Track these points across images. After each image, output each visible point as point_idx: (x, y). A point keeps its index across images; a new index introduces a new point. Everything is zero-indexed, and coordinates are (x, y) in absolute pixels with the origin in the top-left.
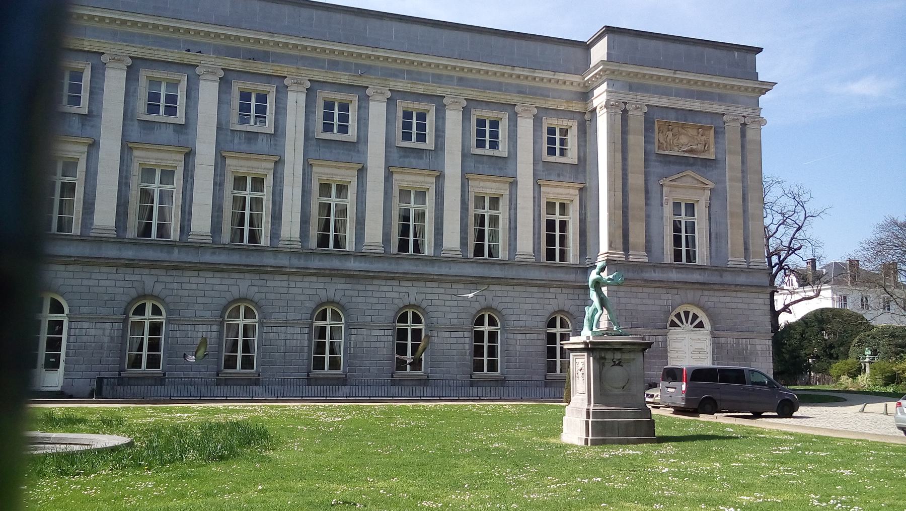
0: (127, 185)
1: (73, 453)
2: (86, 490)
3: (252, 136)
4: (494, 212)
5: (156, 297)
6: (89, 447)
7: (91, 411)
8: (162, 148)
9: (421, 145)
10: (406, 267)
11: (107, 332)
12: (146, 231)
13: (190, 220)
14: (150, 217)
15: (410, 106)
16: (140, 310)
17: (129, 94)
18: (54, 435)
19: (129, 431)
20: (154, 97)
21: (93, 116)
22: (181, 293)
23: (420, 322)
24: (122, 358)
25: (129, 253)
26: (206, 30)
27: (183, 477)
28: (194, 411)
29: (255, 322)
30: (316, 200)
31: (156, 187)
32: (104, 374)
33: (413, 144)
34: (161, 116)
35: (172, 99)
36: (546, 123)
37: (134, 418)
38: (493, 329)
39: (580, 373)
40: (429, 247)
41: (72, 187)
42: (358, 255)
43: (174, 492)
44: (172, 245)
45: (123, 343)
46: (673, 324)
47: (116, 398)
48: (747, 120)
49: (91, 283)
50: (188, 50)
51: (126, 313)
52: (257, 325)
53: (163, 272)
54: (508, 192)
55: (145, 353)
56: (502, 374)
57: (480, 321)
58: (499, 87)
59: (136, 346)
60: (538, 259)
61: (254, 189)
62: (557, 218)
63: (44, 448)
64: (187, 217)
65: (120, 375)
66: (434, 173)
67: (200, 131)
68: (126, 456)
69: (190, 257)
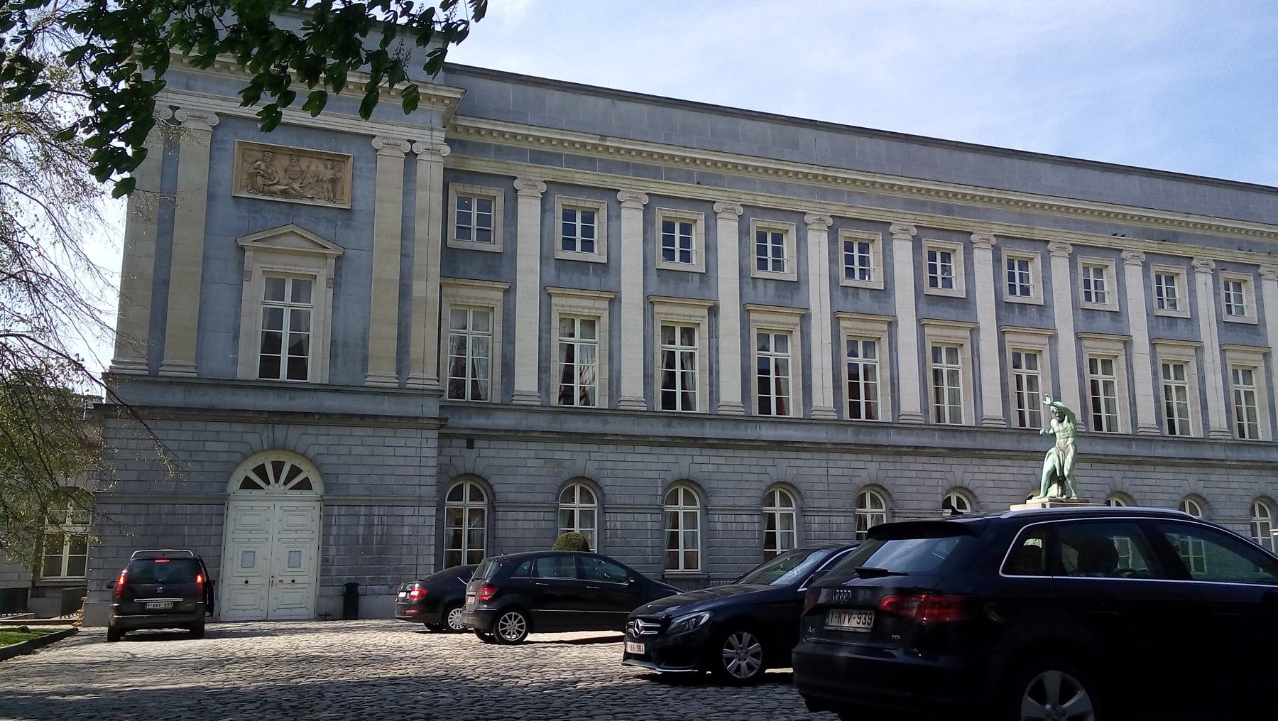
3: (1022, 306)
4: (1108, 378)
10: (768, 433)
15: (673, 214)
33: (578, 254)
36: (928, 244)
42: (806, 422)
46: (248, 484)
52: (486, 509)
56: (704, 571)
58: (590, 163)
61: (1029, 368)
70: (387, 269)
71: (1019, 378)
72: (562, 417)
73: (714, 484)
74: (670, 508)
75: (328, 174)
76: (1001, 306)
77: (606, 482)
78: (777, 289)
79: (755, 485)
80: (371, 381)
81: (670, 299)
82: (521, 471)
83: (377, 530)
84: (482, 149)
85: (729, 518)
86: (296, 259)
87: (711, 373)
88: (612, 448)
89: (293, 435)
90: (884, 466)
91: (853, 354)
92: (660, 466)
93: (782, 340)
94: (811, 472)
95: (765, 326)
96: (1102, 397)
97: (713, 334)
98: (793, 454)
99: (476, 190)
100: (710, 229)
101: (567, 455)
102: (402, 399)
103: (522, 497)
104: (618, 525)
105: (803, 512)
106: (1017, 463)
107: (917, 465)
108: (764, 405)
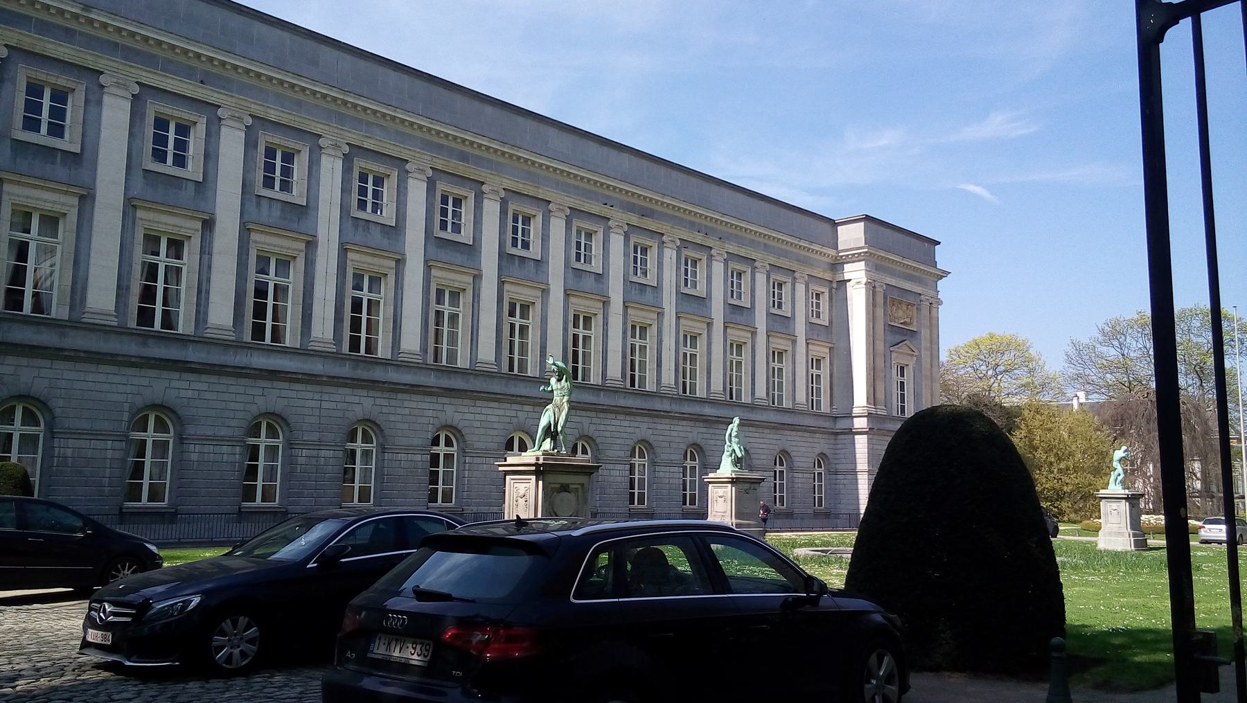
4: (587, 332)
8: (24, 180)
9: (178, 172)
15: (168, 111)
23: (38, 425)
29: (453, 450)
30: (139, 256)
38: (161, 437)
39: (522, 501)
40: (293, 335)
42: (302, 352)
54: (76, 210)
60: (425, 359)
66: (471, 271)
69: (74, 341)
71: (512, 326)
74: (252, 441)
76: (502, 255)
77: (57, 404)
78: (283, 211)
85: (206, 449)
87: (199, 291)
90: (378, 401)
91: (358, 287)
92: (129, 389)
94: (305, 405)
95: (267, 248)
96: (517, 339)
97: (206, 250)
98: (286, 385)
104: (69, 452)
105: (290, 445)
108: (258, 331)
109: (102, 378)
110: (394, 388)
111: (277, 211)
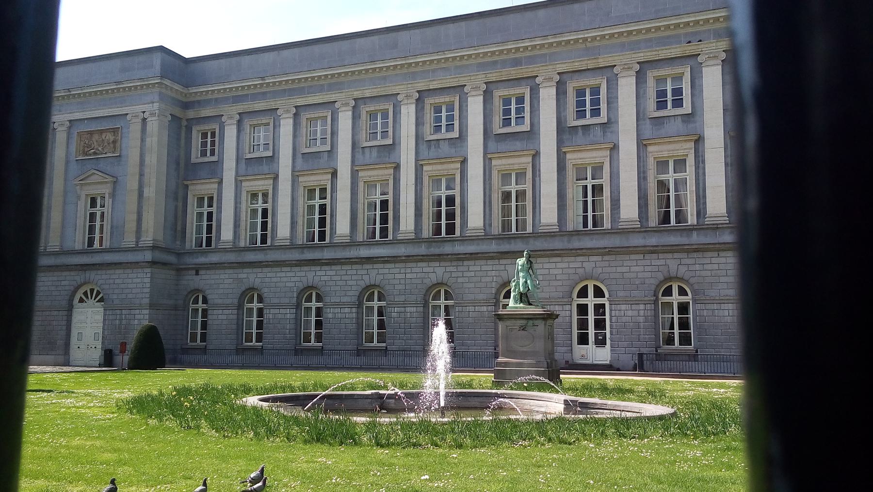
0: (645, 178)
1: (627, 419)
2: (642, 452)
5: (681, 279)
6: (638, 415)
7: (637, 383)
8: (672, 140)
11: (642, 313)
12: (666, 218)
13: (705, 203)
14: (668, 206)
16: (668, 292)
17: (419, 123)
18: (609, 402)
19: (671, 402)
20: (661, 94)
21: (612, 123)
22: (704, 273)
24: (657, 335)
25: (653, 240)
26: (582, 36)
27: (728, 449)
28: (729, 387)
31: (671, 177)
32: (644, 351)
34: (670, 111)
35: (678, 92)
37: (674, 390)
38: (599, 301)
41: (601, 187)
43: (722, 463)
44: (691, 229)
45: (656, 322)
46: (81, 301)
47: (656, 372)
48: (146, 115)
49: (624, 269)
50: (690, 42)
51: (656, 294)
53: (684, 255)
55: (676, 331)
57: (583, 293)
59: (668, 325)
62: (513, 188)
63: (602, 413)
64: (702, 201)
65: (657, 351)
67: (707, 116)
68: (672, 424)
70: (132, 184)
72: (243, 253)
73: (328, 289)
75: (112, 138)
79: (354, 288)
80: (124, 245)
81: (311, 171)
82: (221, 286)
83: (124, 322)
84: (207, 102)
85: (336, 310)
86: (99, 186)
88: (269, 269)
89: (92, 275)
90: (448, 269)
92: (296, 279)
93: (680, 164)
95: (254, 189)
98: (381, 266)
99: (512, 92)
100: (334, 120)
101: (245, 276)
102: (136, 253)
103: (220, 301)
106: (566, 259)
107: (474, 267)
109: (283, 274)
110: (460, 258)
111: (375, 153)
